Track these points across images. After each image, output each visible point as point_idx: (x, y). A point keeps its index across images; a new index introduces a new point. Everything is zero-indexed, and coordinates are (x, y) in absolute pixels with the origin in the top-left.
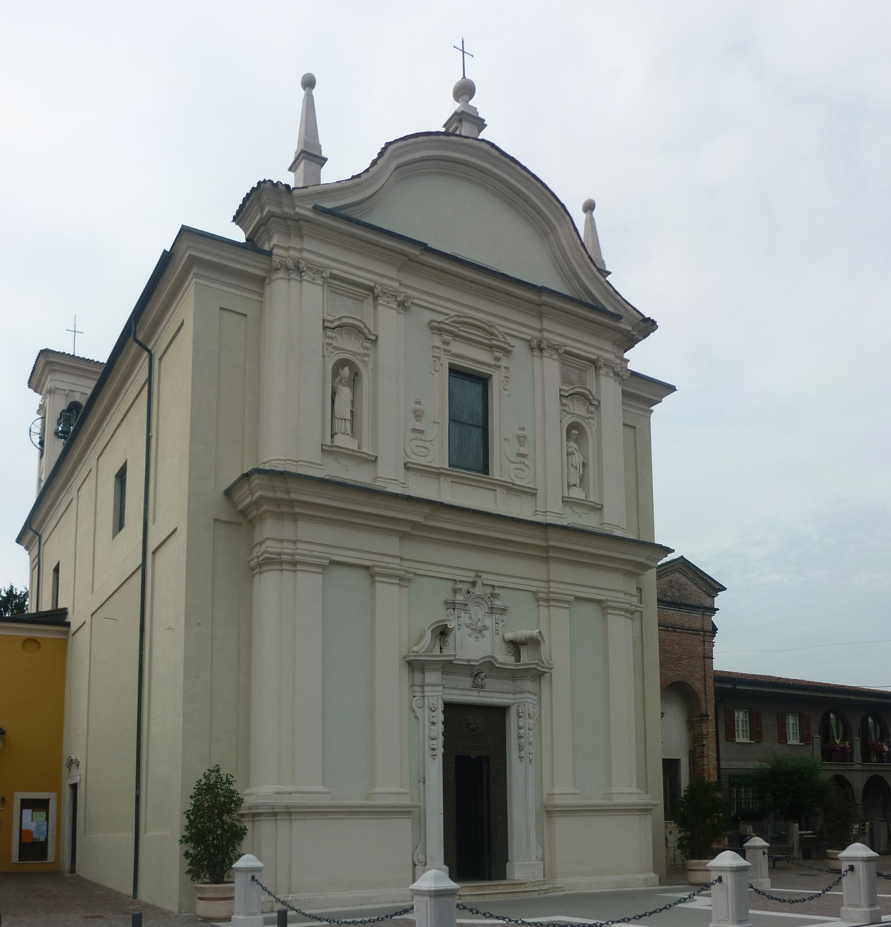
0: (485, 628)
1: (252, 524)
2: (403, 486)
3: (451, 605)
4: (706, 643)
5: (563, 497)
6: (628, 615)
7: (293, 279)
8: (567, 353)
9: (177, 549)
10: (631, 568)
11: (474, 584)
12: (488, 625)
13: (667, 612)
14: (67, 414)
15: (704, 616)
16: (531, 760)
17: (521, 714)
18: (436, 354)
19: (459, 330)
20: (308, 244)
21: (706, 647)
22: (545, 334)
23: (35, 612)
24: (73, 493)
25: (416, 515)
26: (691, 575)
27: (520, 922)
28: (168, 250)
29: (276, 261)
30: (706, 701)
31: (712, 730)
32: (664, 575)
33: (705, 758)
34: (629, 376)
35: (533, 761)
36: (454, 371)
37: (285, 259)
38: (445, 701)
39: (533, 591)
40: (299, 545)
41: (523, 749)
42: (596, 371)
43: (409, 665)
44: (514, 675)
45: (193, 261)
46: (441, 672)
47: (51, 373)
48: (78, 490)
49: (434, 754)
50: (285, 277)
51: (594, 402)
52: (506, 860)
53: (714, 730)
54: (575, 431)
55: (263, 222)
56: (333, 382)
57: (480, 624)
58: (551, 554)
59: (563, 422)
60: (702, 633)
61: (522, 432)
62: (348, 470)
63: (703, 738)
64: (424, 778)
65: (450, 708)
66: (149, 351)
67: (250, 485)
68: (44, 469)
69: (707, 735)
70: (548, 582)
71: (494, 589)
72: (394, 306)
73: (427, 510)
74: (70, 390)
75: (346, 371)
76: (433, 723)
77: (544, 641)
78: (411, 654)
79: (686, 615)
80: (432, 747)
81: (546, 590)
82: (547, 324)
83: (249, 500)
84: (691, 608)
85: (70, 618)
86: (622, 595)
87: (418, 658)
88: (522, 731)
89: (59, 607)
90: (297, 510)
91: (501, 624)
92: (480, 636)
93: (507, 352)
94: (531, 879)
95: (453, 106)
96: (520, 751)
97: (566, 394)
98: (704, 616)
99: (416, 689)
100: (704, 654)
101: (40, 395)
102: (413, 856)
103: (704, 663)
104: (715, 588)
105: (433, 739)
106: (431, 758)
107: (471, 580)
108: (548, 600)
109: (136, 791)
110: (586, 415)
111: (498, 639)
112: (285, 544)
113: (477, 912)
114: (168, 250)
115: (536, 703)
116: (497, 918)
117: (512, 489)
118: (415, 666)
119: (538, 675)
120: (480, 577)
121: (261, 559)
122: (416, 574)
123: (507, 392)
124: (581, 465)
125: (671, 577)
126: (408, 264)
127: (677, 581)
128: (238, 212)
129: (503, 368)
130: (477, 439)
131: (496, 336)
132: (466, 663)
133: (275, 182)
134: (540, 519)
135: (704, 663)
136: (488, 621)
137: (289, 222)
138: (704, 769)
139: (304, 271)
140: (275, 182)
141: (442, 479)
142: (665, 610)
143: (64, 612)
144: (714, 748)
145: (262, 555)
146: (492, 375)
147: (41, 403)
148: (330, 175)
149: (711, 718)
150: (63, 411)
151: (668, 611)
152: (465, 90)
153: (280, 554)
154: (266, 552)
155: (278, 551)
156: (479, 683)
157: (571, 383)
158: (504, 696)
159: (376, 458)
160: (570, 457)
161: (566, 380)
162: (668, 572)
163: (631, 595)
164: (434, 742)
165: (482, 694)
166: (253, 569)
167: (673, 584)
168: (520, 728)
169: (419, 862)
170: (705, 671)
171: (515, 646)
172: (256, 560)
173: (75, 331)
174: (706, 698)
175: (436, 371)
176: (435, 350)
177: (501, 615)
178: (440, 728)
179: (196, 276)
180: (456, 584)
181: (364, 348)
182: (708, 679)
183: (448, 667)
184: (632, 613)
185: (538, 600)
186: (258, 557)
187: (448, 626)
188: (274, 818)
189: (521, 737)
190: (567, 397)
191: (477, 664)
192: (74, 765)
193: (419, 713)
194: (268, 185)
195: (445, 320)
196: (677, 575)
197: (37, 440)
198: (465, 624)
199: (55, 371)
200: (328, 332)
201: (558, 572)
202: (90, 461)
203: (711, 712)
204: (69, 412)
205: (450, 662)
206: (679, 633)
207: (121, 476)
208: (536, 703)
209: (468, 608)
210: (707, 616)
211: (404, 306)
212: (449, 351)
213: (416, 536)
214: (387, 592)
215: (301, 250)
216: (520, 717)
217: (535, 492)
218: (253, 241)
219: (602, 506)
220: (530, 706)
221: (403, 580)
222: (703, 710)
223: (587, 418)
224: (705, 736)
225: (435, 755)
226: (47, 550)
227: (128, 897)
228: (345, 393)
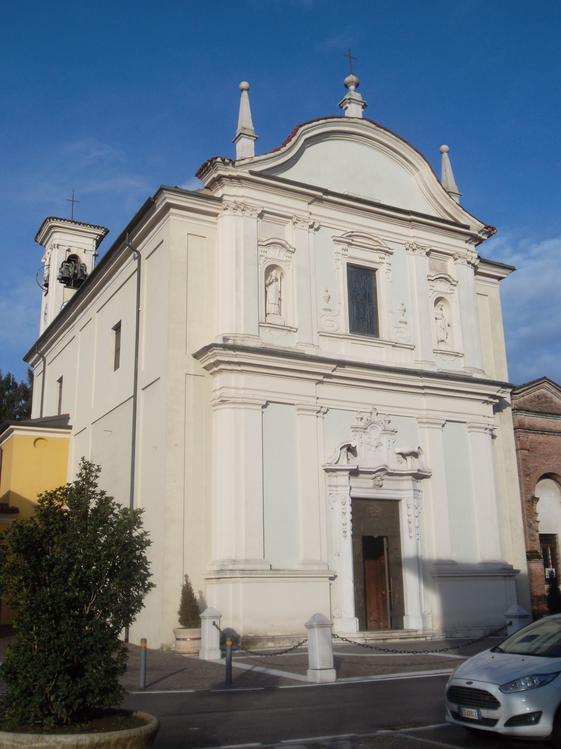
0: (380, 444)
13: (537, 419)
14: (67, 264)
19: (353, 241)
25: (327, 369)
50: (231, 214)
51: (453, 283)
65: (356, 502)
78: (326, 465)
79: (552, 421)
84: (555, 416)
86: (482, 418)
89: (62, 414)
130: (370, 312)
136: (384, 439)
142: (535, 418)
143: (66, 417)
150: (64, 262)
161: (432, 268)
164: (345, 527)
173: (73, 201)
178: (349, 517)
187: (352, 445)
195: (342, 235)
204: (69, 263)
207: (117, 328)
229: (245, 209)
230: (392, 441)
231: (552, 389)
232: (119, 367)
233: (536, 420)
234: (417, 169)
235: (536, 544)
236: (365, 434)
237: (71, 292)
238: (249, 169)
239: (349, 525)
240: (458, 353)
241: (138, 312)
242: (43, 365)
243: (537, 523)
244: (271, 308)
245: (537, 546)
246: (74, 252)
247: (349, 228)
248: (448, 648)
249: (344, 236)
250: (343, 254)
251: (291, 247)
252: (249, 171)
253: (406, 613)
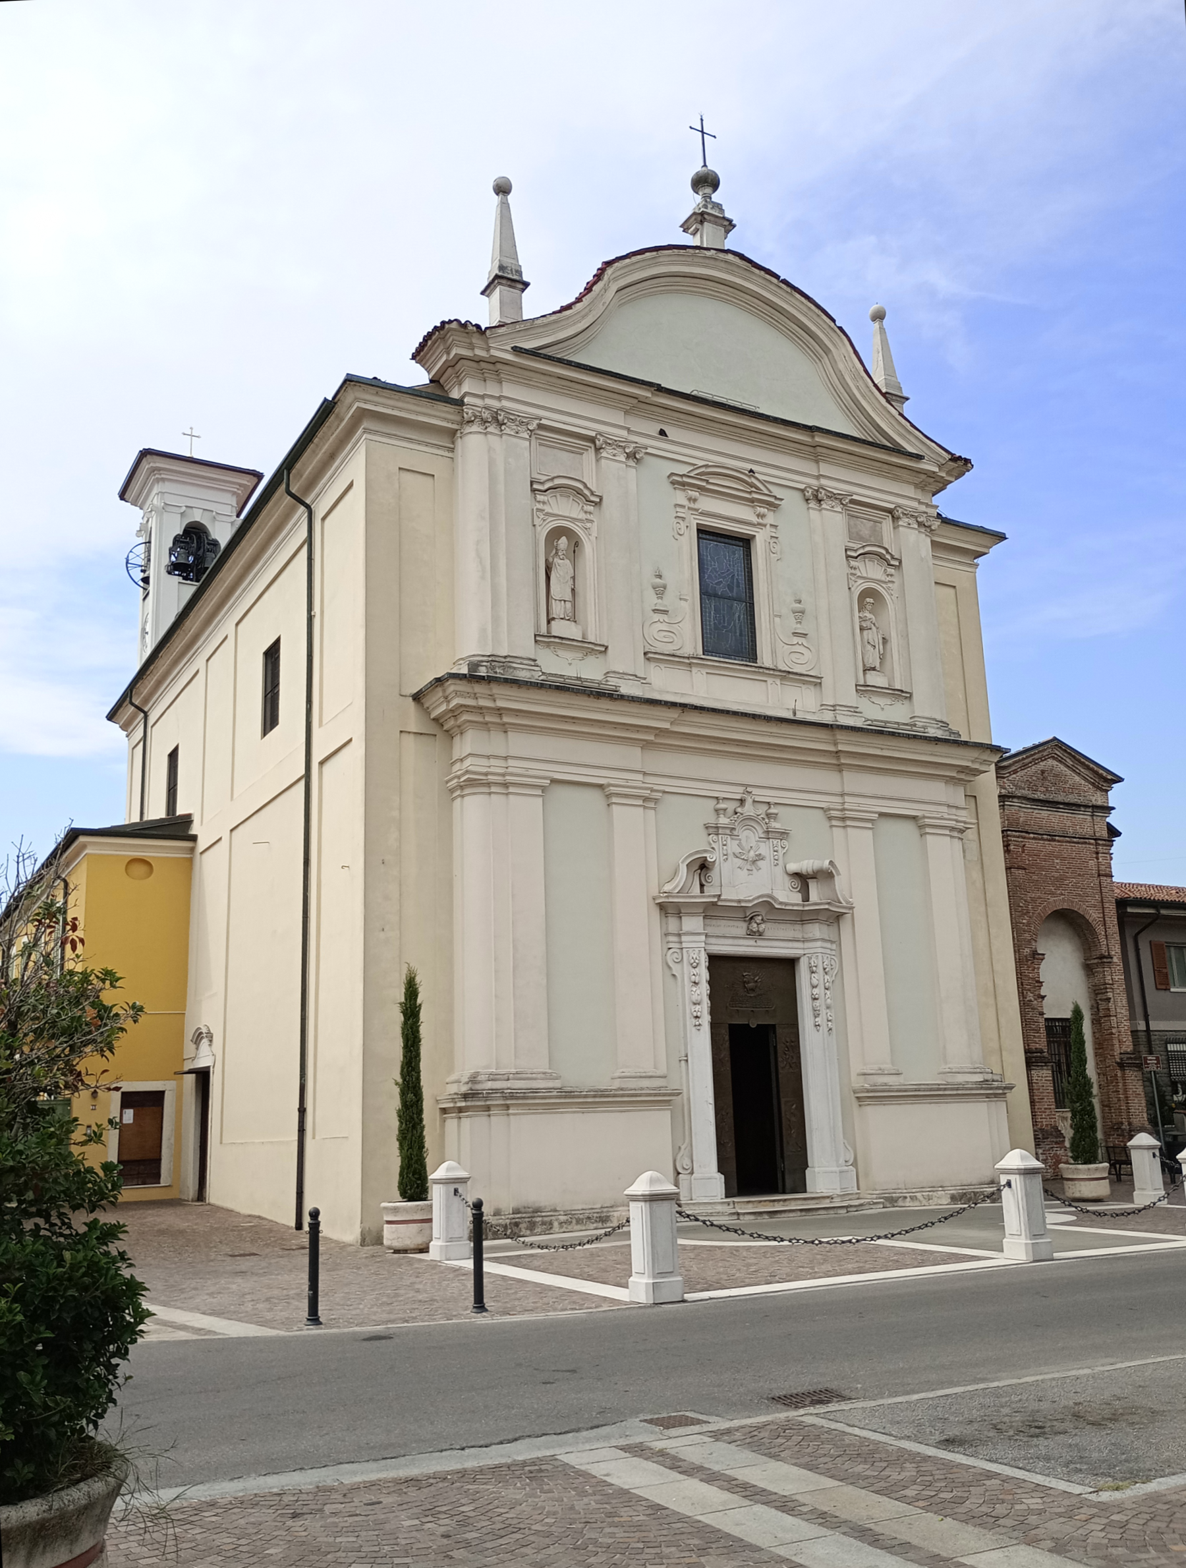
0: (760, 857)
1: (449, 735)
2: (644, 681)
3: (714, 829)
4: (1100, 855)
5: (856, 685)
6: (955, 834)
7: (491, 433)
8: (853, 502)
9: (353, 762)
10: (954, 774)
11: (742, 802)
12: (763, 853)
15: (1095, 818)
16: (830, 1029)
17: (814, 968)
18: (679, 514)
19: (707, 482)
20: (508, 390)
21: (1100, 860)
22: (823, 482)
23: (138, 820)
24: (199, 663)
26: (1070, 762)
27: (794, 1241)
28: (330, 398)
29: (468, 412)
30: (1106, 936)
31: (1119, 977)
32: (1031, 763)
33: (1112, 1018)
34: (938, 526)
35: (834, 1029)
36: (704, 533)
37: (480, 409)
38: (711, 952)
39: (822, 808)
40: (511, 762)
41: (819, 1015)
42: (893, 521)
43: (661, 909)
44: (802, 918)
45: (362, 414)
46: (702, 918)
47: (158, 482)
48: (208, 660)
49: (697, 1023)
51: (893, 562)
52: (805, 1165)
53: (1123, 977)
54: (869, 598)
55: (451, 365)
56: (547, 553)
57: (752, 854)
58: (843, 761)
59: (852, 589)
60: (1092, 841)
61: (798, 605)
62: (570, 664)
63: (1106, 988)
64: (687, 1056)
65: (715, 961)
66: (308, 507)
67: (444, 691)
68: (150, 617)
69: (1112, 984)
70: (842, 795)
71: (770, 808)
72: (622, 458)
73: (674, 714)
74: (186, 507)
75: (563, 542)
76: (695, 983)
77: (839, 874)
80: (695, 1014)
81: (840, 807)
82: (825, 469)
83: (443, 708)
85: (195, 829)
86: (945, 809)
87: (671, 900)
88: (815, 991)
90: (506, 719)
91: (781, 852)
92: (754, 868)
93: (773, 506)
94: (838, 1192)
95: (692, 202)
96: (816, 1017)
97: (855, 554)
98: (1095, 818)
99: (671, 938)
100: (1099, 871)
101: (141, 509)
102: (675, 1161)
103: (1100, 883)
104: (1106, 779)
105: (695, 1004)
106: (694, 1029)
107: (738, 797)
108: (843, 819)
109: (301, 1080)
110: (883, 579)
111: (779, 871)
112: (493, 762)
113: (743, 1233)
114: (330, 398)
115: (833, 953)
116: (767, 1238)
117: (787, 676)
118: (667, 909)
119: (834, 917)
120: (751, 792)
121: (462, 780)
122: (665, 792)
123: (775, 555)
124: (881, 641)
125: (1042, 765)
126: (636, 407)
127: (1052, 770)
128: (422, 346)
129: (768, 526)
130: (739, 617)
131: (757, 488)
132: (736, 904)
133: (463, 322)
134: (827, 718)
135: (1100, 883)
136: (765, 849)
137: (483, 365)
138: (1112, 1034)
139: (505, 424)
140: (463, 322)
141: (694, 670)
142: (1036, 811)
143: (187, 820)
144: (1124, 1002)
145: (463, 775)
146: (755, 536)
147: (141, 521)
148: (534, 305)
149: (1115, 960)
151: (1041, 812)
152: (706, 182)
153: (486, 774)
154: (467, 772)
155: (484, 770)
156: (754, 930)
157: (861, 539)
158: (790, 944)
159: (607, 648)
160: (865, 632)
161: (853, 535)
162: (1037, 759)
163: (957, 808)
164: (698, 1007)
165: (760, 943)
166: (452, 791)
167: (1046, 774)
168: (814, 987)
169: (684, 1168)
170: (1101, 893)
171: (802, 880)
172: (456, 780)
174: (1106, 931)
175: (681, 535)
176: (678, 509)
177: (781, 840)
178: (704, 989)
179: (366, 431)
180: (718, 803)
181: (586, 512)
182: (1106, 905)
183: (712, 911)
184: (962, 831)
185: (830, 818)
186: (459, 777)
187: (709, 859)
188: (487, 1113)
189: (815, 999)
190: (856, 558)
191: (750, 905)
192: (205, 1042)
193: (676, 969)
194: (454, 325)
195: (688, 472)
196: (1051, 762)
197: (138, 575)
198: (734, 854)
199: (163, 480)
200: (538, 496)
201: (855, 782)
202: (226, 626)
203: (1116, 951)
205: (714, 904)
206: (1059, 841)
207: (272, 655)
208: (833, 953)
209: (735, 833)
210: (1099, 818)
211: (635, 458)
212: (697, 510)
213: (661, 744)
214: (627, 816)
215: (499, 398)
216: (813, 972)
217: (819, 681)
218: (438, 381)
219: (911, 694)
220: (825, 958)
221: (649, 801)
222: (1104, 948)
223: (885, 582)
224: (1108, 986)
225: (700, 1025)
226: (155, 734)
227: (289, 1228)
228: (562, 568)
229: (505, 421)
230: (781, 852)
231: (1068, 760)
232: (277, 724)
233: (1038, 816)
234: (827, 351)
235: (1039, 1037)
236: (732, 839)
237: (190, 589)
238: (512, 345)
239: (705, 1009)
240: (902, 691)
241: (310, 619)
242: (143, 726)
243: (1040, 1000)
244: (558, 609)
245: (1041, 1042)
246: (197, 516)
247: (701, 459)
248: (1159, 1203)
249: (692, 474)
250: (689, 508)
251: (592, 493)
252: (512, 348)
253: (809, 1164)
